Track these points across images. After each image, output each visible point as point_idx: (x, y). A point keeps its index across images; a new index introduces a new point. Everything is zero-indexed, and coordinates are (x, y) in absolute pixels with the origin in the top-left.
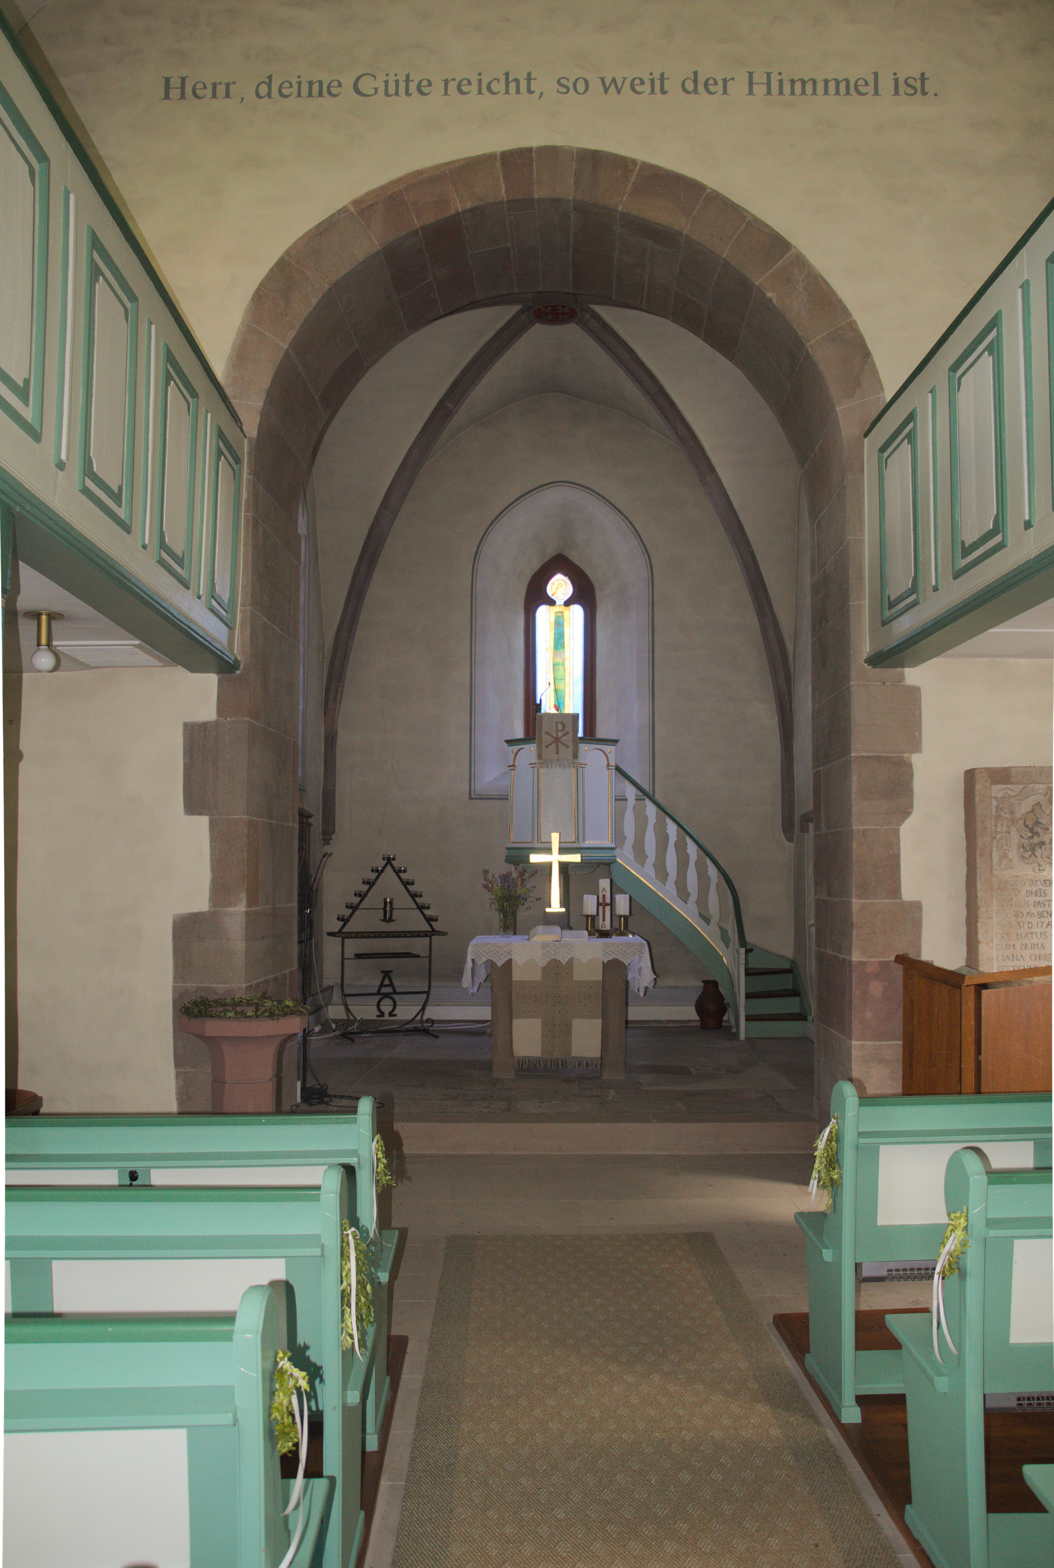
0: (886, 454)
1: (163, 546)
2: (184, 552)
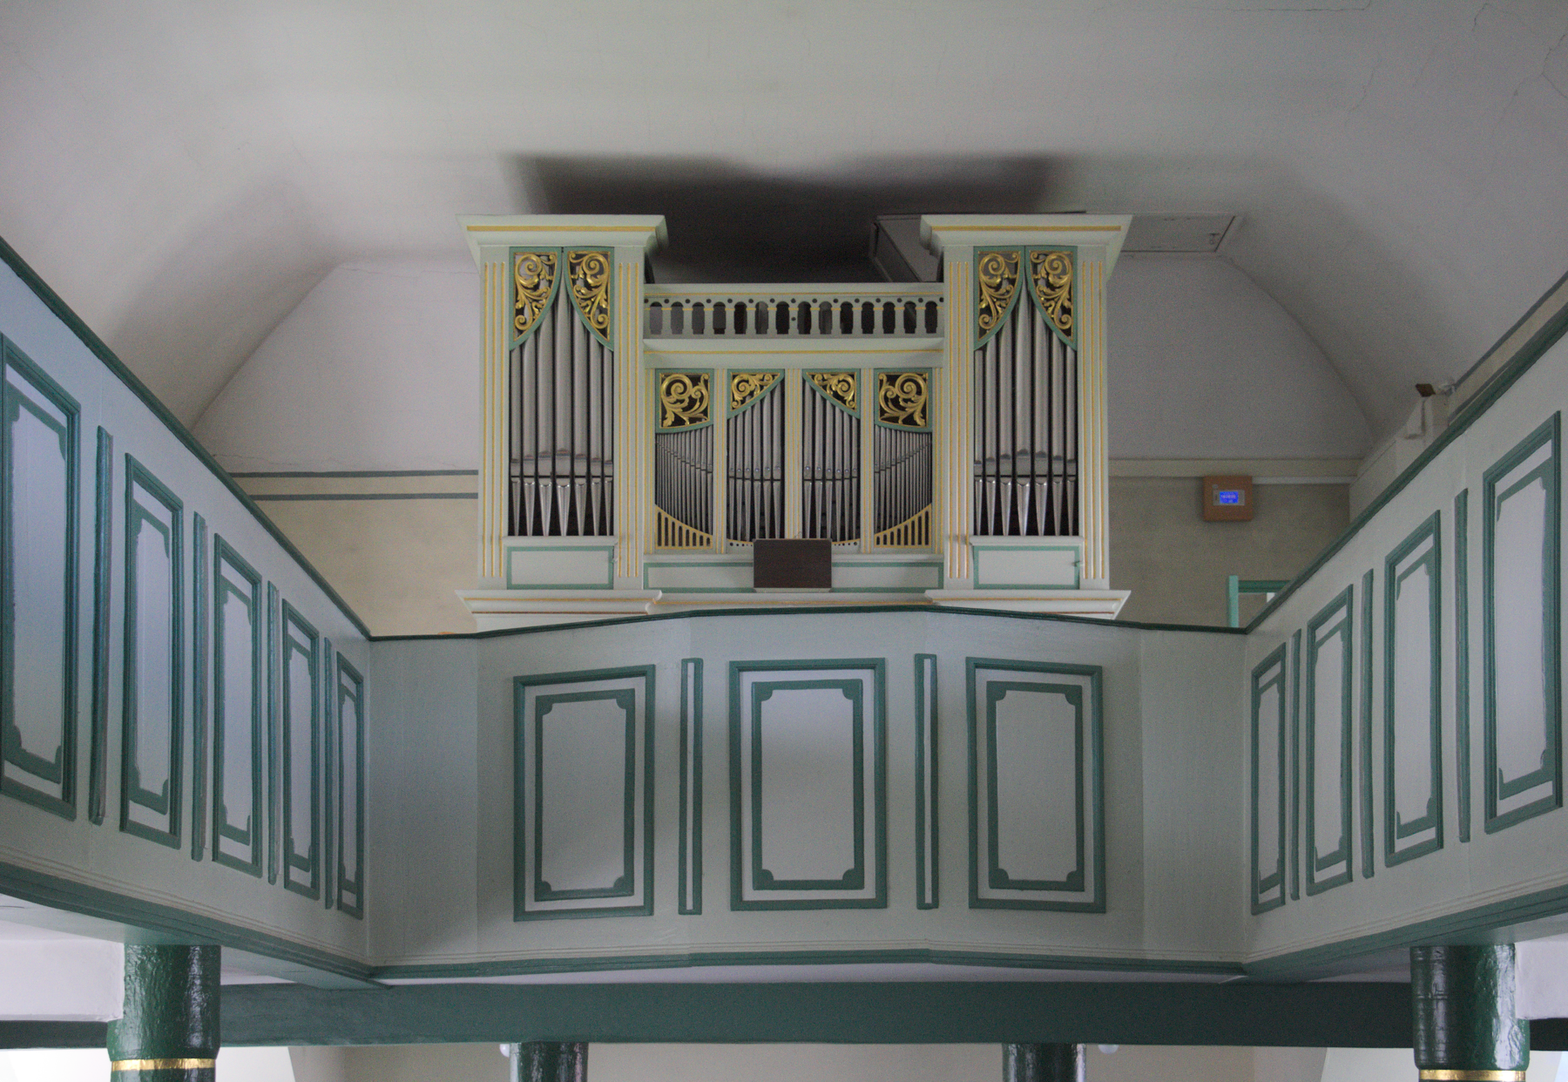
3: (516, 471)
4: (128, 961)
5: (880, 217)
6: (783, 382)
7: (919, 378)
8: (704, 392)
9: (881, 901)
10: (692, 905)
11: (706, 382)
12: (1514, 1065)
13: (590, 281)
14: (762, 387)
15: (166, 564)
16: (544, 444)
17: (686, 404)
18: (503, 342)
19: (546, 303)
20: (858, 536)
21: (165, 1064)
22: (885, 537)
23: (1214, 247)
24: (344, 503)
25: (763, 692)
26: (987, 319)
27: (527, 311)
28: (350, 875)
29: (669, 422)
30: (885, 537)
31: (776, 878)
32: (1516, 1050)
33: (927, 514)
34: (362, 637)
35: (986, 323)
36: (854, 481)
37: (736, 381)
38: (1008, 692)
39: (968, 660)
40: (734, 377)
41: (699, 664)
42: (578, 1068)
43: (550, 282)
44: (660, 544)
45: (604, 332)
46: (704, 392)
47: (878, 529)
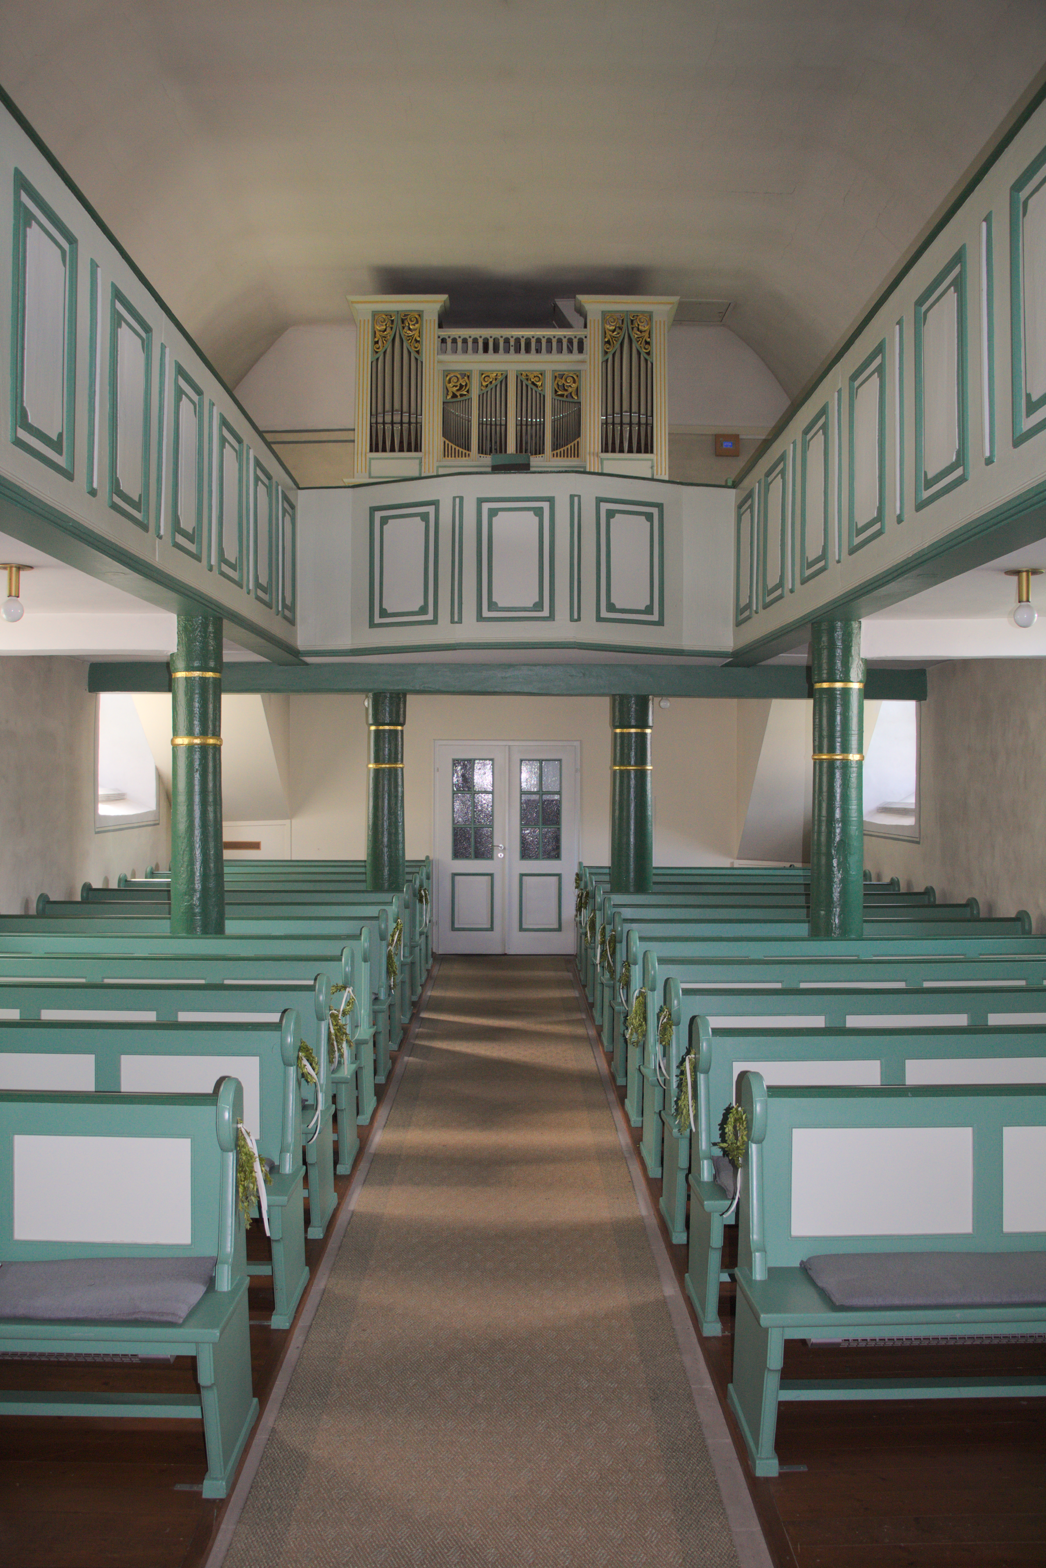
0: (924, 308)
1: (116, 488)
2: (140, 496)
3: (374, 421)
4: (179, 624)
5: (556, 300)
6: (506, 377)
7: (576, 377)
8: (467, 381)
9: (551, 617)
10: (456, 618)
11: (468, 377)
12: (859, 680)
13: (411, 327)
14: (496, 379)
15: (194, 421)
16: (388, 407)
17: (458, 388)
18: (368, 358)
19: (390, 338)
20: (543, 453)
21: (210, 806)
22: (557, 453)
23: (720, 319)
24: (291, 445)
25: (493, 513)
26: (608, 346)
27: (380, 343)
28: (288, 602)
29: (449, 397)
30: (557, 453)
31: (500, 605)
32: (860, 673)
33: (578, 442)
34: (294, 487)
35: (608, 349)
36: (542, 426)
37: (483, 376)
38: (617, 515)
39: (596, 498)
40: (482, 374)
41: (461, 498)
42: (402, 705)
43: (392, 328)
44: (445, 456)
45: (418, 352)
46: (467, 381)
47: (553, 450)
